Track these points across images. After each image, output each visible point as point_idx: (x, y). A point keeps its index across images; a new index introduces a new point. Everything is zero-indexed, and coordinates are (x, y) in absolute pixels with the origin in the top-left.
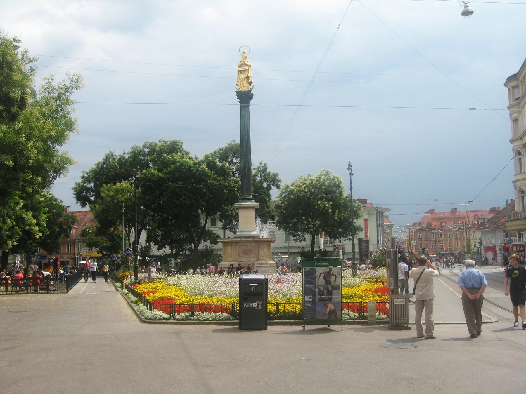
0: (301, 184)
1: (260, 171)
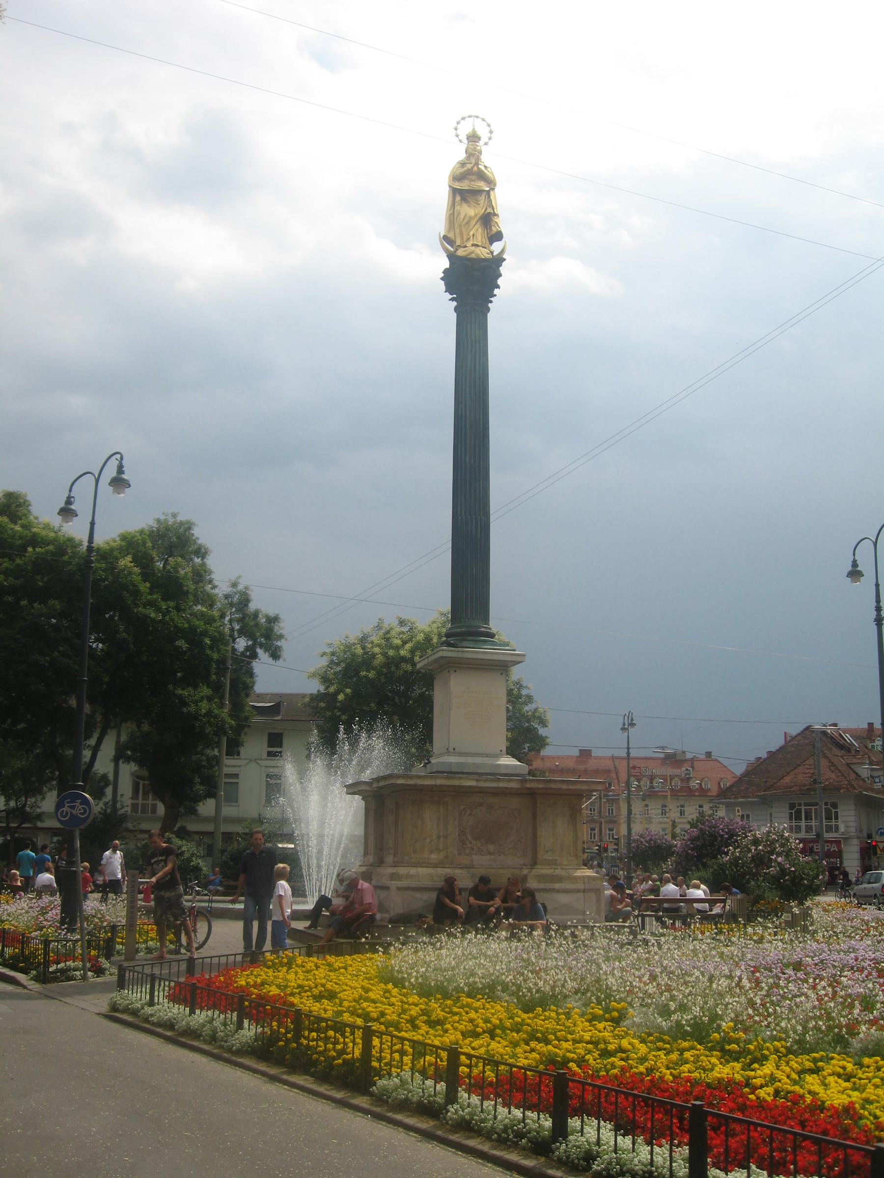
1: (232, 605)
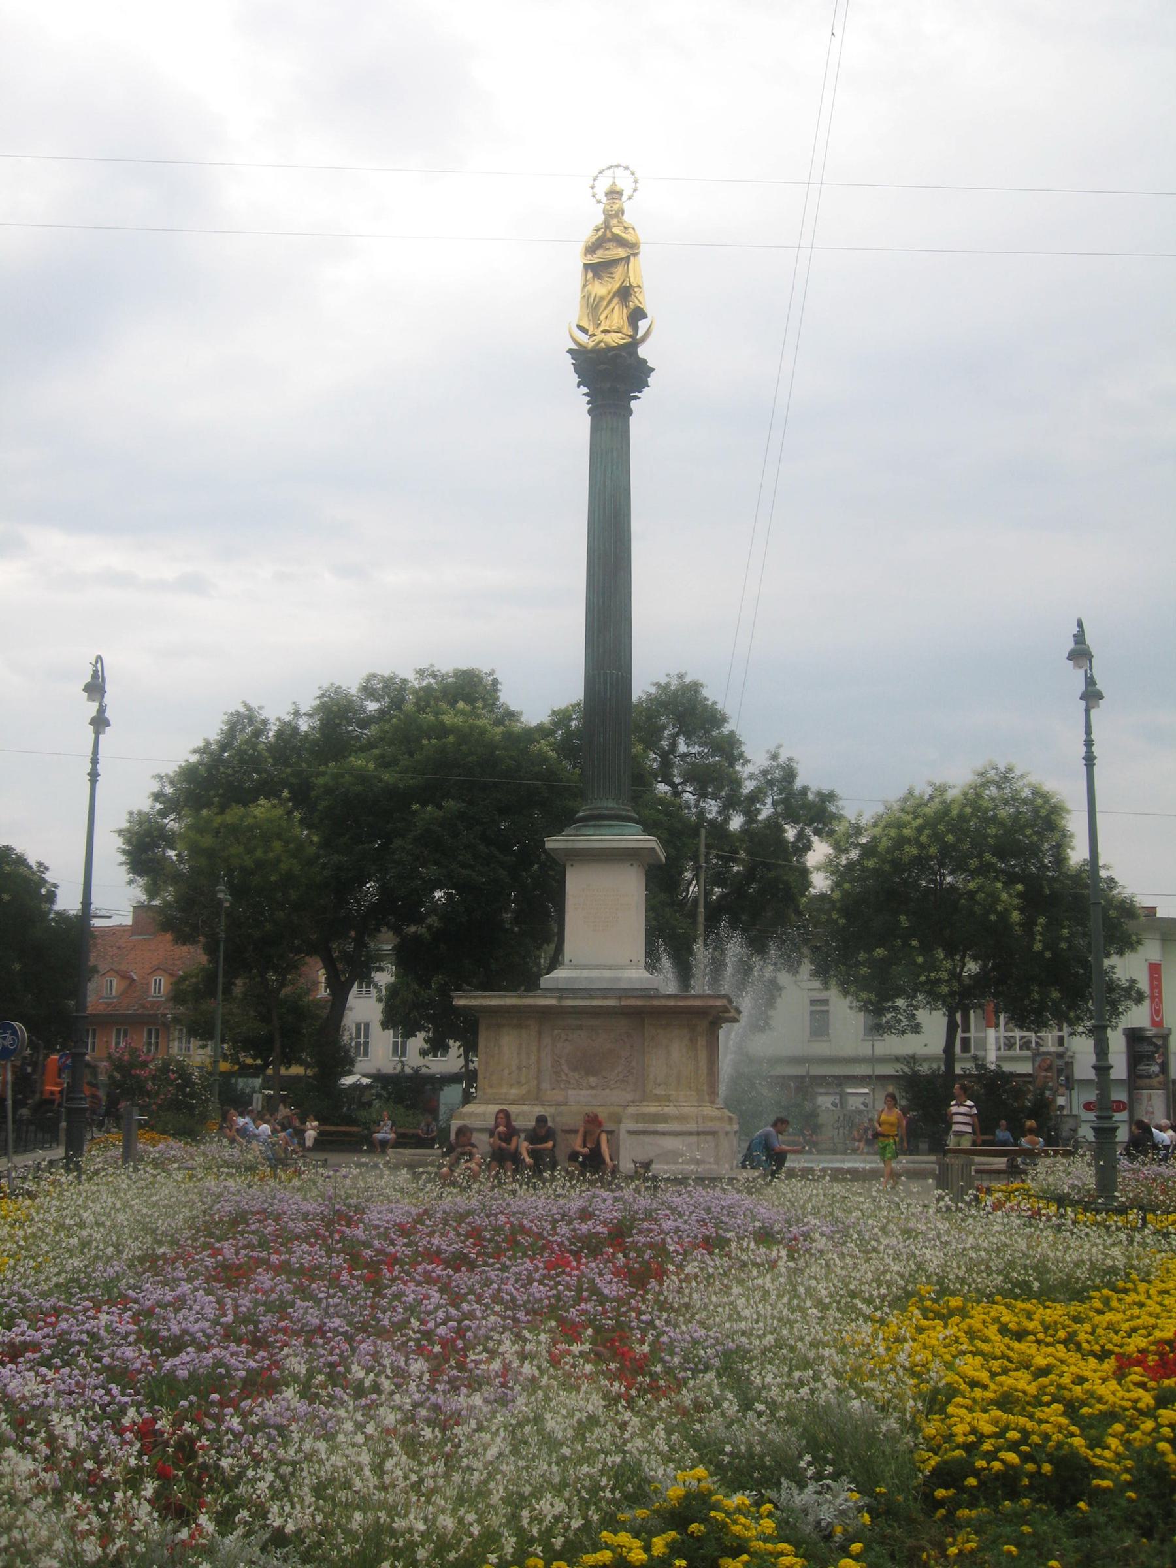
1: (771, 783)
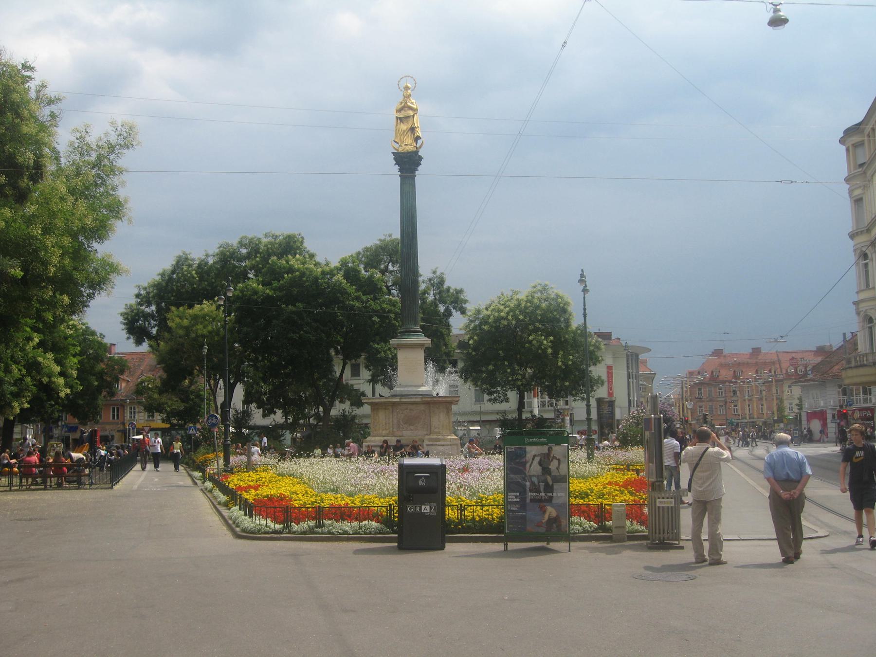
0: (502, 307)
1: (433, 285)
